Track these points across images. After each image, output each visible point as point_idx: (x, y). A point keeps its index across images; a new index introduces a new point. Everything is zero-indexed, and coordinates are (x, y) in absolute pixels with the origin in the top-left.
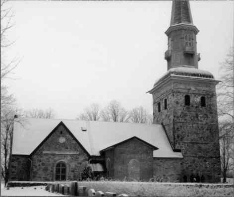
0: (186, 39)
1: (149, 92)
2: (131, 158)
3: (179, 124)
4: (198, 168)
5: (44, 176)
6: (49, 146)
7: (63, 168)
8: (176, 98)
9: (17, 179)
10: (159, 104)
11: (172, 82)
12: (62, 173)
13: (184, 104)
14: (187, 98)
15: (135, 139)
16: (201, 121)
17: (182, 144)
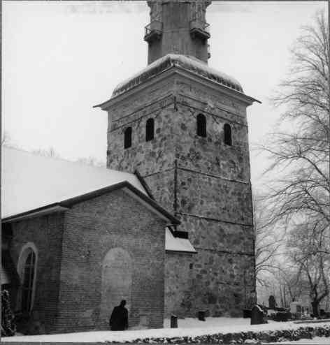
1: (100, 106)
2: (111, 246)
3: (185, 174)
4: (218, 277)
8: (180, 117)
10: (128, 133)
11: (177, 79)
13: (194, 133)
14: (201, 121)
15: (126, 190)
16: (224, 174)
17: (191, 221)
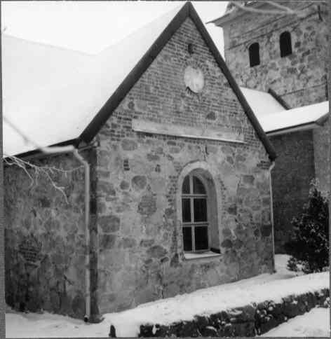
0: (209, 105)
1: (213, 22)
5: (143, 237)
6: (154, 100)
7: (199, 196)
9: (91, 196)
12: (196, 220)
